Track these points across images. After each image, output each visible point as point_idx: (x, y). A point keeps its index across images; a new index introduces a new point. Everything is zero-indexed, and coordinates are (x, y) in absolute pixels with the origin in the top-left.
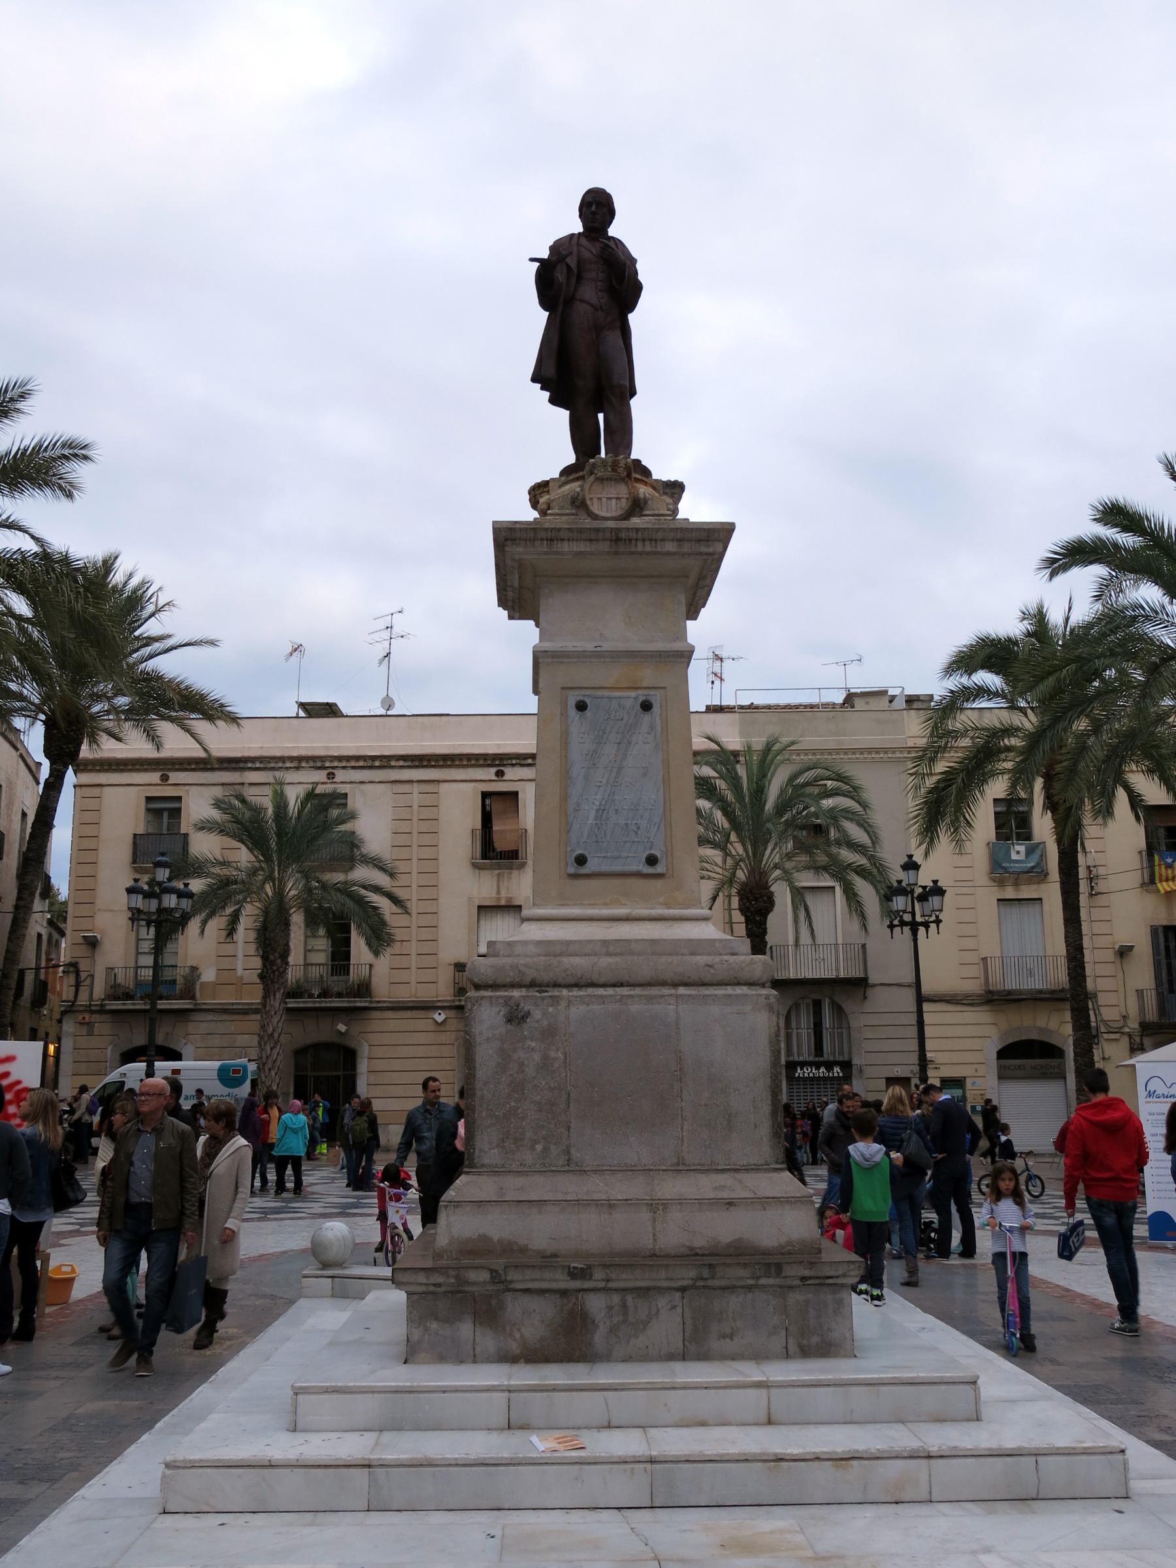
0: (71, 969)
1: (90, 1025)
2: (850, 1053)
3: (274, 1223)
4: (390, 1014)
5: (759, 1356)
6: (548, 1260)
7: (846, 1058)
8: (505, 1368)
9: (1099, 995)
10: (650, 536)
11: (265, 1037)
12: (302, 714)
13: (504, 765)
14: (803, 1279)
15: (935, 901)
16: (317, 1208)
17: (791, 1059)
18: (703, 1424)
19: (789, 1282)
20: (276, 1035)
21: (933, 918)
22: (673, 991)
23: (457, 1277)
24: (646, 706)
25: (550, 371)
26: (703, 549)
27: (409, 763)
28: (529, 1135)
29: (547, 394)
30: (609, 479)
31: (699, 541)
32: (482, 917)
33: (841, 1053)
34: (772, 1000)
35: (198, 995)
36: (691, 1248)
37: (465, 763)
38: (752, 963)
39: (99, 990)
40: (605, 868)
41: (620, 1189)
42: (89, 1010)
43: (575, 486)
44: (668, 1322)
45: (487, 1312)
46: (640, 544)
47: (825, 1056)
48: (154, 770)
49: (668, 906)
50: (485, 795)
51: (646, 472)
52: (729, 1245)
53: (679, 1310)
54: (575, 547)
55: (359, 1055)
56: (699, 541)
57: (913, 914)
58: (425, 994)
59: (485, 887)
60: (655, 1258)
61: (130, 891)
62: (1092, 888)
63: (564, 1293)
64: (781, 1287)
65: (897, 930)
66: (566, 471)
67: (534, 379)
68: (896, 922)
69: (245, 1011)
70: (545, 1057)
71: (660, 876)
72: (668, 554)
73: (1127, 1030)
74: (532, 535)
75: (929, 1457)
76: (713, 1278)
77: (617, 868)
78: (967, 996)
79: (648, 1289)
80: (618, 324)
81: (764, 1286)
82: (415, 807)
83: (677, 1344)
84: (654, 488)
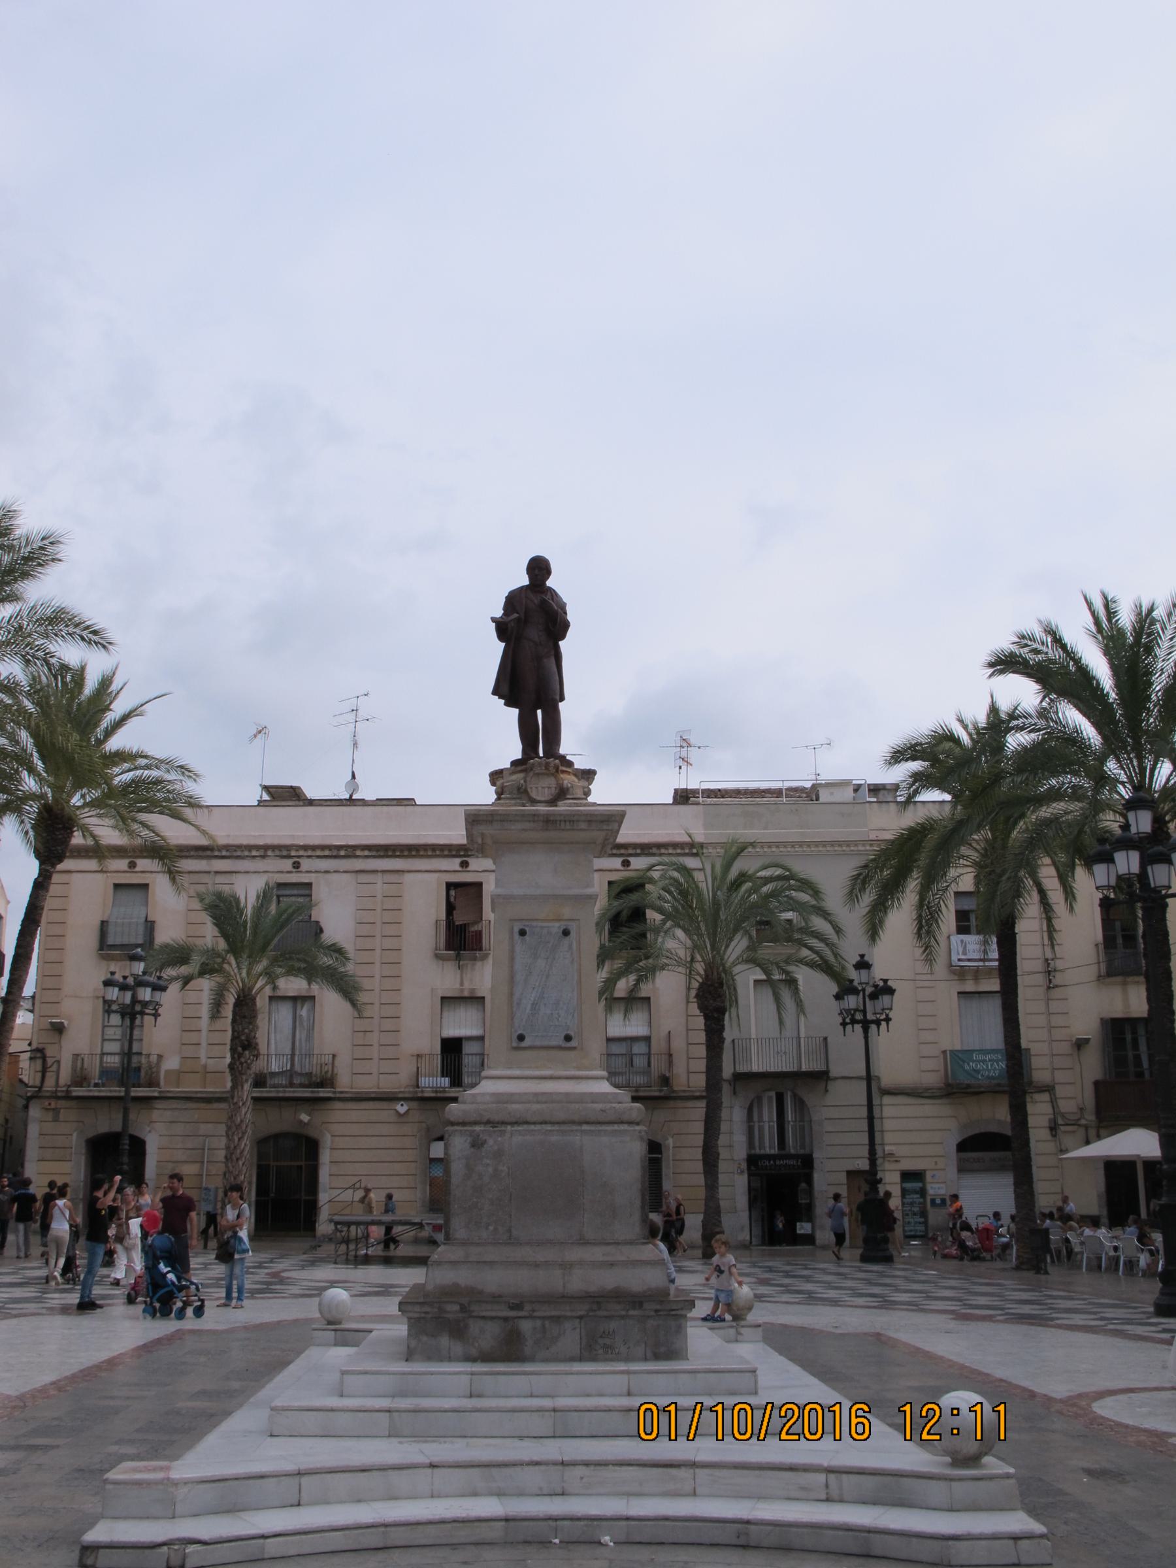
0: (39, 1055)
1: (56, 1111)
5: (628, 1359)
6: (496, 1298)
7: (807, 1151)
8: (469, 1364)
9: (1057, 1087)
10: (571, 820)
11: (233, 1128)
12: (266, 797)
13: (469, 856)
14: (656, 1311)
15: (885, 1000)
16: (295, 1290)
17: (753, 1152)
18: (588, 1396)
21: (883, 1017)
25: (505, 689)
27: (374, 853)
29: (503, 701)
33: (803, 1146)
35: (162, 1083)
38: (631, 1109)
39: (65, 1076)
40: (538, 1043)
41: (542, 1255)
42: (55, 1096)
43: (519, 777)
44: (571, 1337)
45: (457, 1331)
48: (122, 857)
49: (579, 1069)
50: (450, 886)
51: (570, 764)
53: (578, 1330)
54: (519, 826)
57: (864, 1012)
58: (387, 1085)
59: (447, 979)
61: (107, 983)
62: (1050, 981)
63: (506, 1319)
65: (849, 1027)
66: (514, 763)
67: (495, 692)
68: (848, 1020)
71: (574, 1048)
72: (581, 830)
73: (1083, 1122)
76: (599, 1309)
77: (546, 1043)
78: (927, 1089)
80: (553, 652)
84: (575, 775)
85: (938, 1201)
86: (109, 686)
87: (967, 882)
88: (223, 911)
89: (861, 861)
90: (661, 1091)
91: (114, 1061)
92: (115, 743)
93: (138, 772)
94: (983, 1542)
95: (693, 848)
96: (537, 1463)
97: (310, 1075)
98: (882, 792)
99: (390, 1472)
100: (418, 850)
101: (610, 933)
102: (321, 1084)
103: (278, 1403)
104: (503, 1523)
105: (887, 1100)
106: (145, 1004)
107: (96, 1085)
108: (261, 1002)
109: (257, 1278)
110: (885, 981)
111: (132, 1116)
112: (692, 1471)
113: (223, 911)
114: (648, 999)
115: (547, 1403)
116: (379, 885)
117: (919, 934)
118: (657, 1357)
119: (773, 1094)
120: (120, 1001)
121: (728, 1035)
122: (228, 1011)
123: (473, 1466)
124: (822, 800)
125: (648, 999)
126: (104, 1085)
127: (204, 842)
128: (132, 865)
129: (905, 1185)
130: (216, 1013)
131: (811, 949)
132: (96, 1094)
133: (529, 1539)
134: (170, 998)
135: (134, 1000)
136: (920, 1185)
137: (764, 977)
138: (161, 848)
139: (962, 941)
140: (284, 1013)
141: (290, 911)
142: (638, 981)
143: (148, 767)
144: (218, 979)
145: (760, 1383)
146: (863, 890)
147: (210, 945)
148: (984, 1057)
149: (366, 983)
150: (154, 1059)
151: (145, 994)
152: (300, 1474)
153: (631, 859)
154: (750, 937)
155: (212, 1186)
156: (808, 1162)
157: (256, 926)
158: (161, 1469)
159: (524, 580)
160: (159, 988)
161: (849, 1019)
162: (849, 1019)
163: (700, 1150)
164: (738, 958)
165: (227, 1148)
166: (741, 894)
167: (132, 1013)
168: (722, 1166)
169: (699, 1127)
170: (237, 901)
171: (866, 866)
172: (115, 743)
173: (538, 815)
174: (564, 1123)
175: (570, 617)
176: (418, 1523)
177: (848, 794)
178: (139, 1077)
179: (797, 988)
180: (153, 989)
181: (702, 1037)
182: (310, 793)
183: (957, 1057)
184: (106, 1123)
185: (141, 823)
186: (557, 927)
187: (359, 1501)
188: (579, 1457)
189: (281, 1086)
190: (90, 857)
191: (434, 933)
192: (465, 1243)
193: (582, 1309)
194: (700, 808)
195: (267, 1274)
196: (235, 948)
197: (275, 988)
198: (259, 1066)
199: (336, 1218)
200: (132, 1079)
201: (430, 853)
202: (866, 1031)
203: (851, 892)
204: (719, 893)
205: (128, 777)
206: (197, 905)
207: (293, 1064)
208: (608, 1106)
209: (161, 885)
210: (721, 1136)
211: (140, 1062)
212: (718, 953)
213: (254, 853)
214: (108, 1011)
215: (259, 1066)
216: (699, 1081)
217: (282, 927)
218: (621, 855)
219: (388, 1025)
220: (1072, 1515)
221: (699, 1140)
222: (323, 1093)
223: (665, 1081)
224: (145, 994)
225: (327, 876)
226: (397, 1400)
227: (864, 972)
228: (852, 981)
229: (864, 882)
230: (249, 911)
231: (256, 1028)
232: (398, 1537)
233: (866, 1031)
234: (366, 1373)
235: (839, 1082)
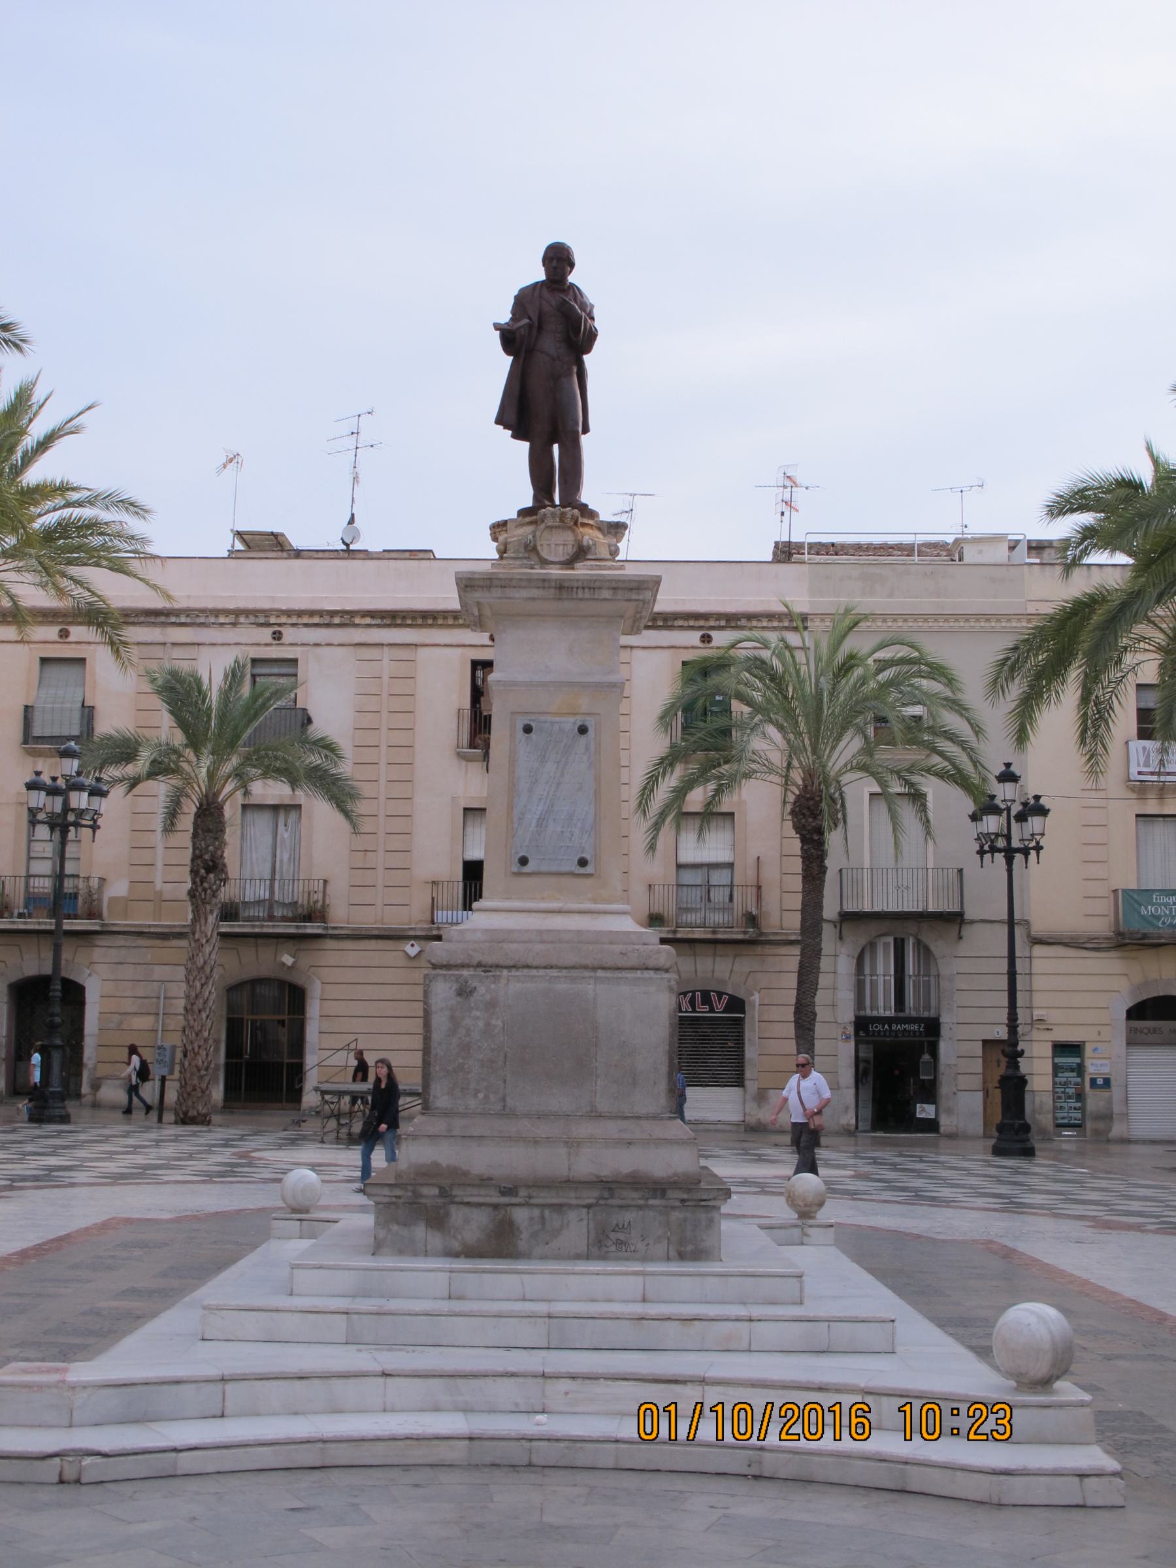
2: (938, 1008)
3: (218, 1186)
4: (348, 944)
5: (645, 1259)
6: (484, 1182)
7: (933, 1014)
8: (449, 1260)
10: (592, 586)
11: (196, 972)
12: (239, 546)
14: (683, 1201)
17: (862, 1013)
18: (593, 1300)
19: (671, 1203)
20: (208, 970)
21: (1033, 844)
22: (592, 974)
23: (414, 1192)
24: (583, 730)
25: (512, 417)
26: (634, 597)
27: (378, 621)
28: (473, 1086)
29: (510, 432)
30: (559, 527)
31: (631, 589)
32: (469, 823)
33: (928, 1007)
34: (673, 983)
36: (598, 1177)
37: (450, 622)
38: (658, 952)
41: (543, 1129)
44: (576, 1229)
45: (437, 1220)
46: (580, 591)
47: (907, 1011)
48: (51, 623)
49: (595, 901)
51: (592, 514)
52: (627, 1176)
53: (585, 1222)
54: (524, 593)
55: (309, 994)
56: (631, 589)
57: (1008, 838)
58: (394, 919)
60: (570, 1183)
61: (31, 786)
63: (496, 1207)
64: (666, 1207)
65: (988, 856)
66: (523, 513)
67: (499, 421)
68: (986, 848)
70: (488, 1024)
72: (605, 600)
74: (488, 583)
75: (751, 1320)
76: (612, 1197)
77: (554, 868)
78: (1091, 939)
79: (561, 1205)
81: (652, 1206)
82: (385, 679)
83: (582, 1246)
84: (599, 529)
85: (1100, 1082)
86: (29, 399)
87: (1149, 672)
88: (180, 693)
89: (1009, 641)
90: (745, 933)
91: (44, 885)
92: (33, 476)
93: (66, 512)
94: (1042, 1479)
95: (798, 621)
96: (513, 1375)
98: (1047, 551)
99: (334, 1381)
100: (435, 618)
101: (684, 728)
102: (308, 917)
103: (212, 1302)
104: (467, 1442)
105: (1038, 950)
106: (81, 813)
107: (21, 916)
108: (231, 811)
109: (220, 1159)
110: (1037, 798)
111: (66, 955)
112: (700, 1388)
113: (180, 693)
114: (732, 814)
115: (542, 1308)
116: (386, 663)
117: (1083, 740)
118: (682, 1257)
119: (890, 940)
120: (49, 809)
121: (832, 863)
122: (186, 822)
123: (434, 1376)
124: (966, 560)
125: (732, 814)
126: (30, 916)
127: (159, 604)
128: (64, 634)
129: (1057, 1060)
130: (170, 825)
131: (941, 754)
132: (22, 927)
133: (498, 1461)
134: (114, 807)
135: (66, 809)
136: (1078, 1060)
137: (878, 790)
138: (99, 611)
139: (1144, 748)
140: (261, 824)
141: (268, 694)
142: (719, 791)
143: (79, 504)
144: (173, 782)
145: (807, 1291)
146: (1010, 678)
147: (163, 739)
148: (1166, 900)
149: (366, 790)
150: (94, 883)
151: (80, 800)
152: (223, 1380)
153: (713, 633)
154: (866, 737)
155: (167, 1045)
156: (933, 1027)
157: (222, 717)
158: (57, 1370)
159: (540, 275)
160: (97, 792)
161: (987, 847)
162: (987, 847)
163: (793, 1009)
164: (846, 765)
165: (188, 997)
166: (852, 681)
168: (819, 1030)
169: (792, 980)
170: (198, 682)
171: (1015, 649)
172: (33, 476)
173: (549, 580)
174: (573, 967)
175: (598, 324)
176: (363, 1440)
177: (1001, 553)
178: (75, 905)
179: (924, 806)
180: (91, 794)
181: (797, 865)
182: (297, 541)
183: (1132, 899)
184: (33, 963)
185: (71, 578)
186: (570, 724)
187: (296, 1413)
188: (563, 1370)
189: (258, 919)
190: (9, 623)
191: (455, 726)
192: (448, 1114)
193: (590, 1196)
194: (805, 568)
195: (234, 1154)
196: (195, 742)
197: (247, 793)
198: (226, 893)
199: (325, 1087)
201: (450, 622)
202: (1009, 861)
203: (995, 681)
204: (822, 679)
205: (51, 519)
206: (147, 687)
207: (272, 892)
208: (630, 948)
209: (101, 659)
210: (819, 992)
211: (77, 887)
212: (819, 758)
213: (222, 620)
214: (33, 822)
215: (226, 893)
216: (794, 921)
217: (255, 716)
218: (700, 628)
219: (396, 843)
220: (1166, 1454)
221: (791, 997)
222: (312, 928)
223: (752, 920)
224: (80, 800)
225: (318, 650)
226: (358, 1300)
227: (1009, 786)
228: (993, 797)
229: (1012, 669)
230: (214, 697)
231: (224, 843)
233: (1009, 861)
234: (321, 1267)
235: (976, 926)
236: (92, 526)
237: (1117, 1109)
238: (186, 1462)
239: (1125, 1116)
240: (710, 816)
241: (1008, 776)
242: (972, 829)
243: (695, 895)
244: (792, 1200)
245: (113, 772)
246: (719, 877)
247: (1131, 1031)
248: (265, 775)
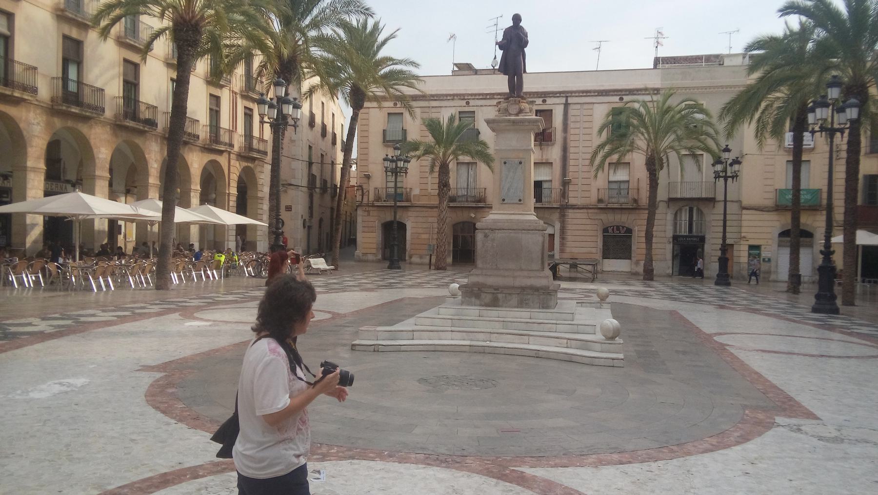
6: (490, 287)
11: (441, 221)
12: (456, 69)
15: (736, 167)
39: (372, 197)
44: (515, 300)
45: (478, 297)
60: (513, 287)
61: (385, 160)
69: (432, 207)
88: (433, 126)
91: (392, 191)
92: (381, 54)
97: (475, 196)
102: (479, 201)
105: (744, 212)
106: (401, 168)
108: (452, 166)
113: (433, 126)
117: (756, 136)
118: (543, 308)
122: (437, 169)
129: (751, 252)
134: (413, 166)
140: (463, 170)
143: (396, 64)
156: (702, 239)
157: (447, 134)
160: (407, 161)
162: (717, 176)
167: (396, 172)
172: (381, 54)
182: (477, 66)
184: (388, 217)
186: (517, 161)
192: (482, 269)
196: (438, 142)
200: (399, 200)
203: (721, 116)
215: (450, 193)
224: (401, 164)
232: (440, 348)
236: (401, 72)
237: (772, 269)
238: (403, 348)
239: (776, 272)
240: (617, 165)
241: (727, 150)
242: (712, 170)
243: (615, 192)
244: (598, 295)
245: (413, 154)
246: (623, 186)
247: (780, 241)
248: (462, 154)
